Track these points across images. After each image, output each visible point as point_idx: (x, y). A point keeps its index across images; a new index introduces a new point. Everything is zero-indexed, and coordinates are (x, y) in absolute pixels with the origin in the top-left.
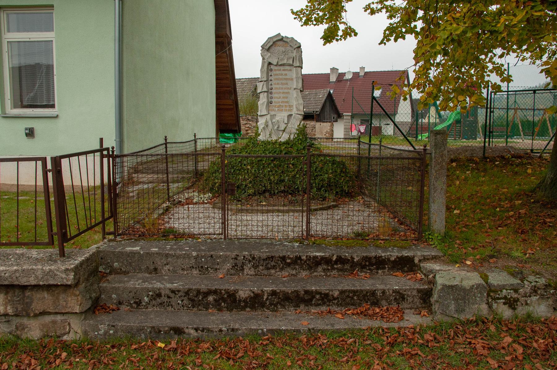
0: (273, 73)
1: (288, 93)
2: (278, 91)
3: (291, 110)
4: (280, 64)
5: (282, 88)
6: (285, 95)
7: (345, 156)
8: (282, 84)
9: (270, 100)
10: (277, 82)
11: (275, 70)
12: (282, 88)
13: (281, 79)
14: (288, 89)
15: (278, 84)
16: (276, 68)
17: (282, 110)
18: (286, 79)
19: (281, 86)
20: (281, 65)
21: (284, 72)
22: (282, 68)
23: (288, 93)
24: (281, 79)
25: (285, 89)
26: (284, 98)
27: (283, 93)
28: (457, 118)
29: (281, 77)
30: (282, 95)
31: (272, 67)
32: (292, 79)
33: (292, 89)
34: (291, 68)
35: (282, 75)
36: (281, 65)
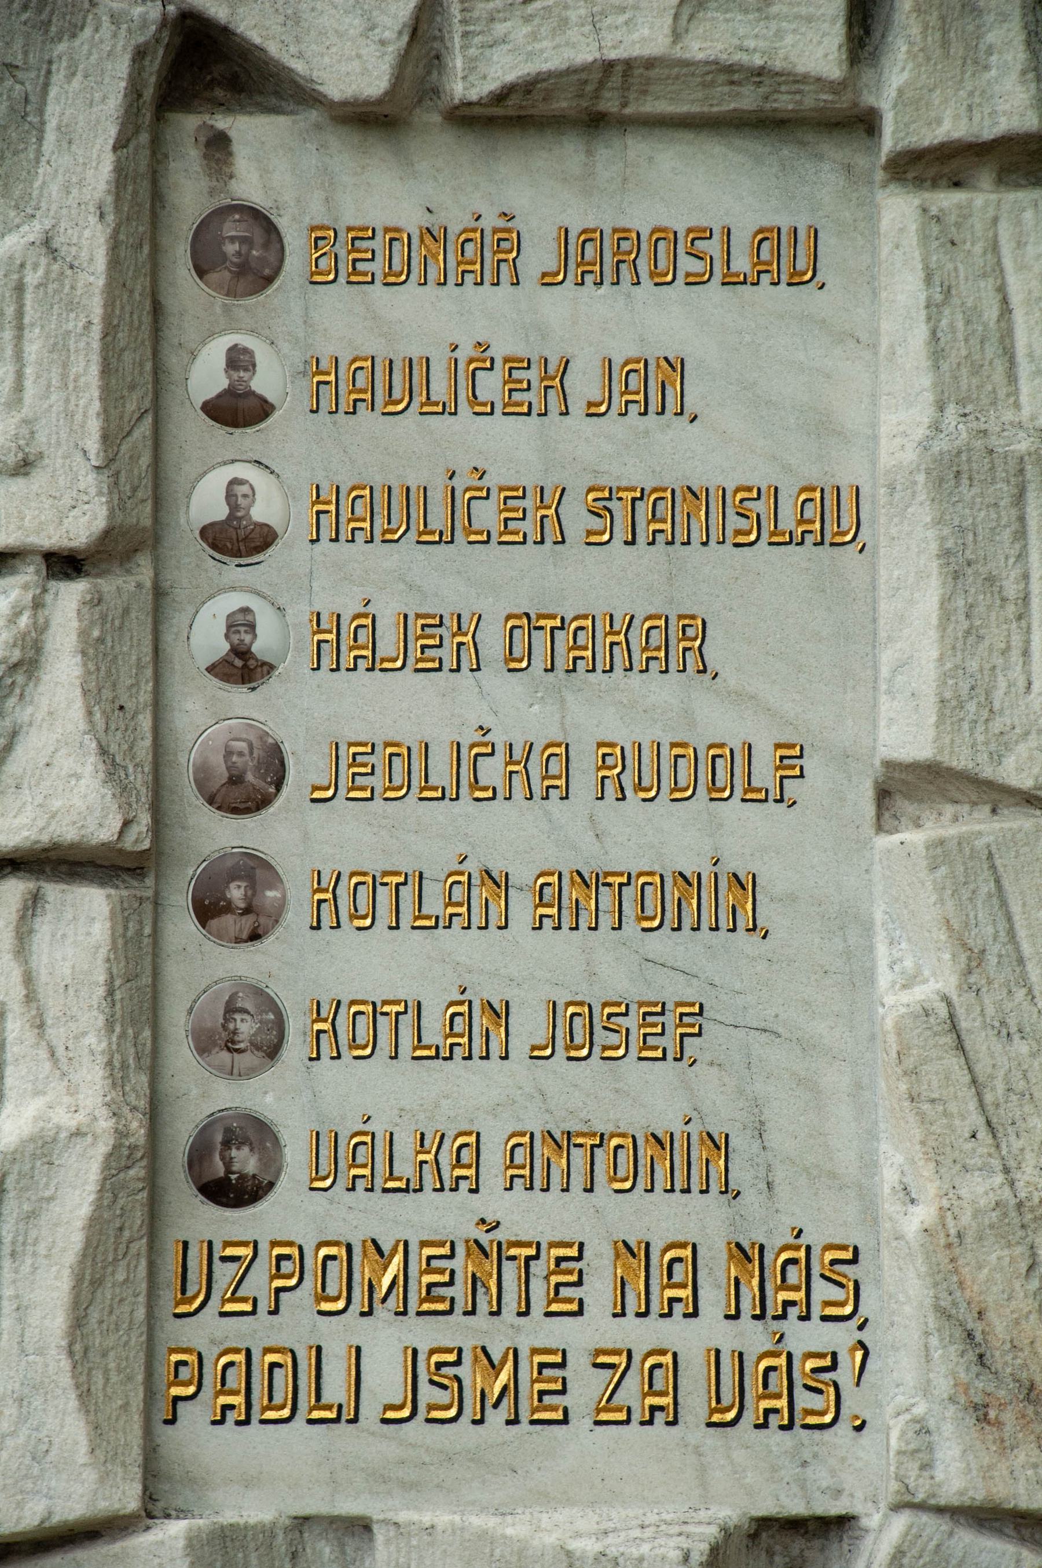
0: (293, 331)
1: (725, 900)
2: (429, 837)
3: (796, 1399)
4: (478, 71)
5: (543, 772)
6: (610, 965)
7: (874, 609)
8: (555, 643)
9: (203, 1094)
10: (391, 579)
11: (354, 256)
12: (543, 772)
13: (532, 517)
14: (716, 774)
15: (437, 644)
16: (383, 193)
17: (536, 1397)
18: (660, 515)
19: (515, 708)
20: (515, 115)
21: (598, 326)
22: (541, 194)
23: (725, 900)
24: (532, 517)
25: (624, 775)
26: (583, 1030)
27: (575, 897)
28: (29, 710)
29: (508, 448)
30: (532, 966)
31: (269, 161)
32: (829, 521)
33: (842, 792)
34: (808, 190)
35: (536, 386)
36: (515, 115)
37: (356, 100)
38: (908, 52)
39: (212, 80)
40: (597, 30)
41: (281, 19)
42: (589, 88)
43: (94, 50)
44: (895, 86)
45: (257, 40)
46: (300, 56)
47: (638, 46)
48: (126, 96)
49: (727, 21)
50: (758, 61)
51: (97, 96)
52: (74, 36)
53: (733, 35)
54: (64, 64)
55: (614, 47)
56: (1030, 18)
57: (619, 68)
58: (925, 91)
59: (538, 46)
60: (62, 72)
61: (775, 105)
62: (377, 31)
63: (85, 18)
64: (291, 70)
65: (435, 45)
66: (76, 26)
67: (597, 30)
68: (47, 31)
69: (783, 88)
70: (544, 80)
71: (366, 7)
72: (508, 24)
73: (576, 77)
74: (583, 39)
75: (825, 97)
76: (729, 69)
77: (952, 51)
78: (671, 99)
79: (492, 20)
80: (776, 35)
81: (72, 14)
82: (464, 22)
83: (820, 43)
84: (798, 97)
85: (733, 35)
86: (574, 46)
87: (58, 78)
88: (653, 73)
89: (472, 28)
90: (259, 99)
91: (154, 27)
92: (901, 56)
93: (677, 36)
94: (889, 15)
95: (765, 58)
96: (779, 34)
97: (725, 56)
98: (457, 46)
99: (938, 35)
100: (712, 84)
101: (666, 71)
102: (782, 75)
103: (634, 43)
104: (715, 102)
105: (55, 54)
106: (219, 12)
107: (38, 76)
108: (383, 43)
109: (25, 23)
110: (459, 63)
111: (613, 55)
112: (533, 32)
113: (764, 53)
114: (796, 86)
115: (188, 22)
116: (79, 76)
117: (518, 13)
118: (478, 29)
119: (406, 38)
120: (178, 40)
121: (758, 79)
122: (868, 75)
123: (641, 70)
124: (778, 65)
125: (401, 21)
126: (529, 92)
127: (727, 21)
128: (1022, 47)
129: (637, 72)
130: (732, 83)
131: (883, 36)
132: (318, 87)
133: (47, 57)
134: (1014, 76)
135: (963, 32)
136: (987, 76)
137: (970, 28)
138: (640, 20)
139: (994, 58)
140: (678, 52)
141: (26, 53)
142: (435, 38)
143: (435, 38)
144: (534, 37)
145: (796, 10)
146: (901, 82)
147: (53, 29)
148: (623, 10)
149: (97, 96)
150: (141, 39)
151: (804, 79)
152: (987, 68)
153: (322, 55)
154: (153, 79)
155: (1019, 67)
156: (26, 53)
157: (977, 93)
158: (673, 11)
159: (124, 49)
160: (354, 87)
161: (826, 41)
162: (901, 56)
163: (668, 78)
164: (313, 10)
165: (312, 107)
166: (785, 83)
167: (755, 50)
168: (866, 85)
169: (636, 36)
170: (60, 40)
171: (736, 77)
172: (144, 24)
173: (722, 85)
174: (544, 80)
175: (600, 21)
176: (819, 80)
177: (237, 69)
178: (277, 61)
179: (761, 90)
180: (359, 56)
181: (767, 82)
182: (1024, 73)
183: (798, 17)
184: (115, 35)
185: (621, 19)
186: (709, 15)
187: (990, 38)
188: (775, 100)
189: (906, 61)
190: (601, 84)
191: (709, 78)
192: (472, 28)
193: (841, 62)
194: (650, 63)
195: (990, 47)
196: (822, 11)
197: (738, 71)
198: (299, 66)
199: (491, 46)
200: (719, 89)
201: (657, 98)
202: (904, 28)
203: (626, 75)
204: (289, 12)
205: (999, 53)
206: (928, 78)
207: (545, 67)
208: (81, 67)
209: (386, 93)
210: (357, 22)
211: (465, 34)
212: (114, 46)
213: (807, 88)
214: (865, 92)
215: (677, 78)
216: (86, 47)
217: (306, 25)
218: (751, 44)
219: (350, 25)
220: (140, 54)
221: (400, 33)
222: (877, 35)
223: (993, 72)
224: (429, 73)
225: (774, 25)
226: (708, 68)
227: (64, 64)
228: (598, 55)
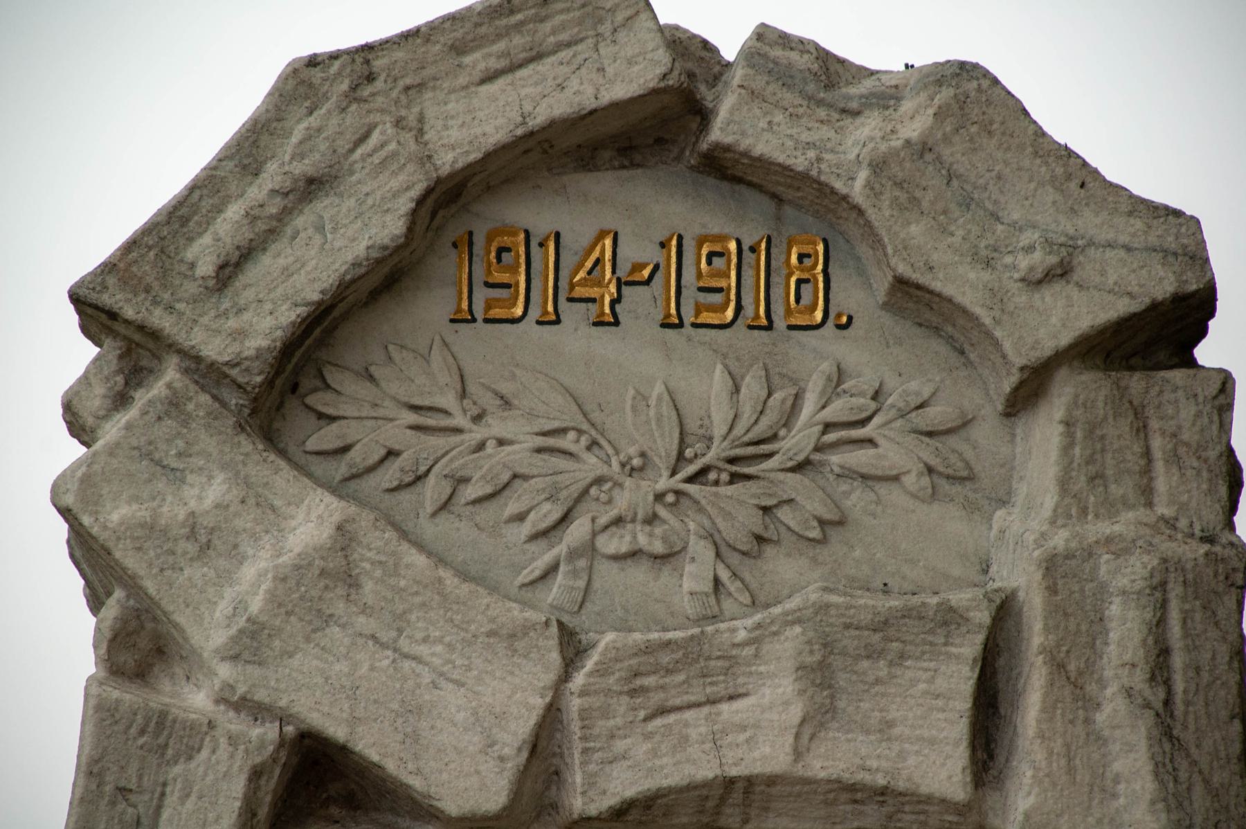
37: (474, 815)
38: (1033, 777)
39: (328, 798)
40: (718, 748)
41: (400, 737)
42: (710, 804)
43: (210, 772)
44: (1021, 810)
45: (375, 758)
46: (418, 772)
47: (759, 763)
48: (240, 815)
49: (849, 741)
50: (881, 781)
51: (211, 816)
52: (190, 758)
53: (855, 754)
54: (179, 786)
55: (735, 765)
56: (1156, 749)
57: (740, 785)
58: (1053, 816)
59: (658, 763)
60: (177, 794)
61: (899, 825)
62: (496, 748)
63: (202, 740)
64: (408, 786)
65: (554, 761)
66: (193, 748)
67: (718, 748)
68: (163, 755)
69: (907, 808)
70: (665, 796)
71: (486, 725)
72: (629, 741)
73: (697, 793)
74: (703, 756)
75: (950, 818)
76: (852, 788)
77: (1078, 778)
78: (794, 816)
79: (613, 737)
80: (898, 756)
81: (190, 736)
82: (584, 738)
83: (943, 765)
84: (922, 817)
85: (855, 754)
86: (694, 762)
87: (171, 800)
88: (774, 790)
89: (592, 744)
90: (374, 815)
91: (271, 748)
92: (1027, 780)
93: (798, 754)
94: (1012, 741)
95: (888, 778)
96: (902, 755)
97: (847, 775)
98: (577, 762)
99: (1063, 762)
100: (834, 802)
101: (788, 789)
102: (905, 795)
103: (755, 760)
104: (838, 820)
105: (171, 776)
106: (337, 732)
107: (151, 799)
108: (502, 759)
109: (141, 747)
110: (578, 779)
111: (734, 772)
112: (653, 749)
113: (887, 773)
114: (921, 807)
115: (307, 741)
116: (193, 798)
117: (638, 730)
118: (598, 745)
119: (525, 754)
120: (295, 760)
121: (881, 799)
122: (992, 799)
123: (762, 787)
124: (901, 785)
125: (520, 738)
126: (649, 807)
127: (849, 741)
128: (1149, 778)
129: (758, 789)
130: (856, 801)
131: (1007, 760)
132: (435, 803)
133: (161, 780)
134: (1144, 805)
135: (1089, 759)
136: (1115, 804)
137: (1096, 756)
138: (761, 739)
139: (1122, 787)
140: (799, 770)
141: (140, 777)
142: (554, 755)
143: (554, 755)
144: (654, 753)
145: (918, 732)
146: (1027, 806)
147: (170, 752)
148: (743, 728)
149: (211, 816)
150: (258, 760)
151: (929, 799)
152: (1115, 796)
153: (441, 772)
154: (268, 798)
155: (1148, 797)
156: (140, 777)
157: (1106, 821)
158: (794, 731)
159: (241, 769)
160: (472, 802)
161: (949, 763)
162: (1027, 780)
163: (790, 795)
164: (432, 728)
165: (428, 823)
166: (908, 802)
167: (877, 770)
168: (992, 808)
169: (756, 754)
170: (176, 763)
171: (859, 796)
172: (262, 745)
173: (845, 803)
174: (665, 796)
175: (721, 739)
176: (943, 801)
177: (353, 786)
178: (395, 778)
179: (884, 810)
180: (478, 772)
181: (890, 801)
182: (1153, 803)
183: (920, 739)
184: (232, 756)
185: (742, 738)
186: (831, 734)
187: (1117, 766)
188: (899, 820)
189: (1031, 785)
190: (722, 800)
191: (831, 796)
192: (592, 744)
193: (965, 784)
194: (772, 780)
195: (1117, 775)
196: (945, 734)
197: (861, 790)
198: (416, 783)
199: (611, 762)
200: (841, 807)
201: (780, 815)
202: (1029, 754)
203: (747, 792)
204: (409, 730)
205: (1128, 782)
206: (1056, 803)
207: (665, 783)
208: (196, 788)
209: (504, 809)
210: (476, 739)
211: (585, 751)
212: (231, 766)
213: (931, 809)
214: (991, 815)
215: (799, 795)
216: (201, 769)
217: (425, 742)
218: (874, 764)
219: (469, 742)
220: (256, 774)
221: (520, 749)
222: (1001, 759)
223: (1122, 801)
224: (548, 788)
225: (896, 747)
226: (830, 786)
227: (179, 786)
228: (719, 772)
